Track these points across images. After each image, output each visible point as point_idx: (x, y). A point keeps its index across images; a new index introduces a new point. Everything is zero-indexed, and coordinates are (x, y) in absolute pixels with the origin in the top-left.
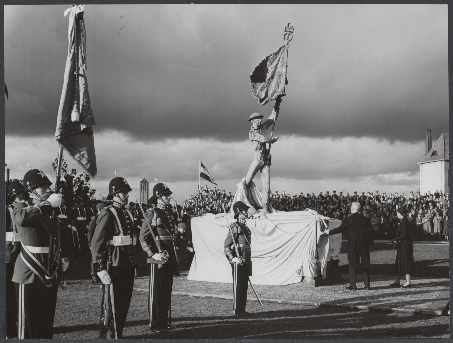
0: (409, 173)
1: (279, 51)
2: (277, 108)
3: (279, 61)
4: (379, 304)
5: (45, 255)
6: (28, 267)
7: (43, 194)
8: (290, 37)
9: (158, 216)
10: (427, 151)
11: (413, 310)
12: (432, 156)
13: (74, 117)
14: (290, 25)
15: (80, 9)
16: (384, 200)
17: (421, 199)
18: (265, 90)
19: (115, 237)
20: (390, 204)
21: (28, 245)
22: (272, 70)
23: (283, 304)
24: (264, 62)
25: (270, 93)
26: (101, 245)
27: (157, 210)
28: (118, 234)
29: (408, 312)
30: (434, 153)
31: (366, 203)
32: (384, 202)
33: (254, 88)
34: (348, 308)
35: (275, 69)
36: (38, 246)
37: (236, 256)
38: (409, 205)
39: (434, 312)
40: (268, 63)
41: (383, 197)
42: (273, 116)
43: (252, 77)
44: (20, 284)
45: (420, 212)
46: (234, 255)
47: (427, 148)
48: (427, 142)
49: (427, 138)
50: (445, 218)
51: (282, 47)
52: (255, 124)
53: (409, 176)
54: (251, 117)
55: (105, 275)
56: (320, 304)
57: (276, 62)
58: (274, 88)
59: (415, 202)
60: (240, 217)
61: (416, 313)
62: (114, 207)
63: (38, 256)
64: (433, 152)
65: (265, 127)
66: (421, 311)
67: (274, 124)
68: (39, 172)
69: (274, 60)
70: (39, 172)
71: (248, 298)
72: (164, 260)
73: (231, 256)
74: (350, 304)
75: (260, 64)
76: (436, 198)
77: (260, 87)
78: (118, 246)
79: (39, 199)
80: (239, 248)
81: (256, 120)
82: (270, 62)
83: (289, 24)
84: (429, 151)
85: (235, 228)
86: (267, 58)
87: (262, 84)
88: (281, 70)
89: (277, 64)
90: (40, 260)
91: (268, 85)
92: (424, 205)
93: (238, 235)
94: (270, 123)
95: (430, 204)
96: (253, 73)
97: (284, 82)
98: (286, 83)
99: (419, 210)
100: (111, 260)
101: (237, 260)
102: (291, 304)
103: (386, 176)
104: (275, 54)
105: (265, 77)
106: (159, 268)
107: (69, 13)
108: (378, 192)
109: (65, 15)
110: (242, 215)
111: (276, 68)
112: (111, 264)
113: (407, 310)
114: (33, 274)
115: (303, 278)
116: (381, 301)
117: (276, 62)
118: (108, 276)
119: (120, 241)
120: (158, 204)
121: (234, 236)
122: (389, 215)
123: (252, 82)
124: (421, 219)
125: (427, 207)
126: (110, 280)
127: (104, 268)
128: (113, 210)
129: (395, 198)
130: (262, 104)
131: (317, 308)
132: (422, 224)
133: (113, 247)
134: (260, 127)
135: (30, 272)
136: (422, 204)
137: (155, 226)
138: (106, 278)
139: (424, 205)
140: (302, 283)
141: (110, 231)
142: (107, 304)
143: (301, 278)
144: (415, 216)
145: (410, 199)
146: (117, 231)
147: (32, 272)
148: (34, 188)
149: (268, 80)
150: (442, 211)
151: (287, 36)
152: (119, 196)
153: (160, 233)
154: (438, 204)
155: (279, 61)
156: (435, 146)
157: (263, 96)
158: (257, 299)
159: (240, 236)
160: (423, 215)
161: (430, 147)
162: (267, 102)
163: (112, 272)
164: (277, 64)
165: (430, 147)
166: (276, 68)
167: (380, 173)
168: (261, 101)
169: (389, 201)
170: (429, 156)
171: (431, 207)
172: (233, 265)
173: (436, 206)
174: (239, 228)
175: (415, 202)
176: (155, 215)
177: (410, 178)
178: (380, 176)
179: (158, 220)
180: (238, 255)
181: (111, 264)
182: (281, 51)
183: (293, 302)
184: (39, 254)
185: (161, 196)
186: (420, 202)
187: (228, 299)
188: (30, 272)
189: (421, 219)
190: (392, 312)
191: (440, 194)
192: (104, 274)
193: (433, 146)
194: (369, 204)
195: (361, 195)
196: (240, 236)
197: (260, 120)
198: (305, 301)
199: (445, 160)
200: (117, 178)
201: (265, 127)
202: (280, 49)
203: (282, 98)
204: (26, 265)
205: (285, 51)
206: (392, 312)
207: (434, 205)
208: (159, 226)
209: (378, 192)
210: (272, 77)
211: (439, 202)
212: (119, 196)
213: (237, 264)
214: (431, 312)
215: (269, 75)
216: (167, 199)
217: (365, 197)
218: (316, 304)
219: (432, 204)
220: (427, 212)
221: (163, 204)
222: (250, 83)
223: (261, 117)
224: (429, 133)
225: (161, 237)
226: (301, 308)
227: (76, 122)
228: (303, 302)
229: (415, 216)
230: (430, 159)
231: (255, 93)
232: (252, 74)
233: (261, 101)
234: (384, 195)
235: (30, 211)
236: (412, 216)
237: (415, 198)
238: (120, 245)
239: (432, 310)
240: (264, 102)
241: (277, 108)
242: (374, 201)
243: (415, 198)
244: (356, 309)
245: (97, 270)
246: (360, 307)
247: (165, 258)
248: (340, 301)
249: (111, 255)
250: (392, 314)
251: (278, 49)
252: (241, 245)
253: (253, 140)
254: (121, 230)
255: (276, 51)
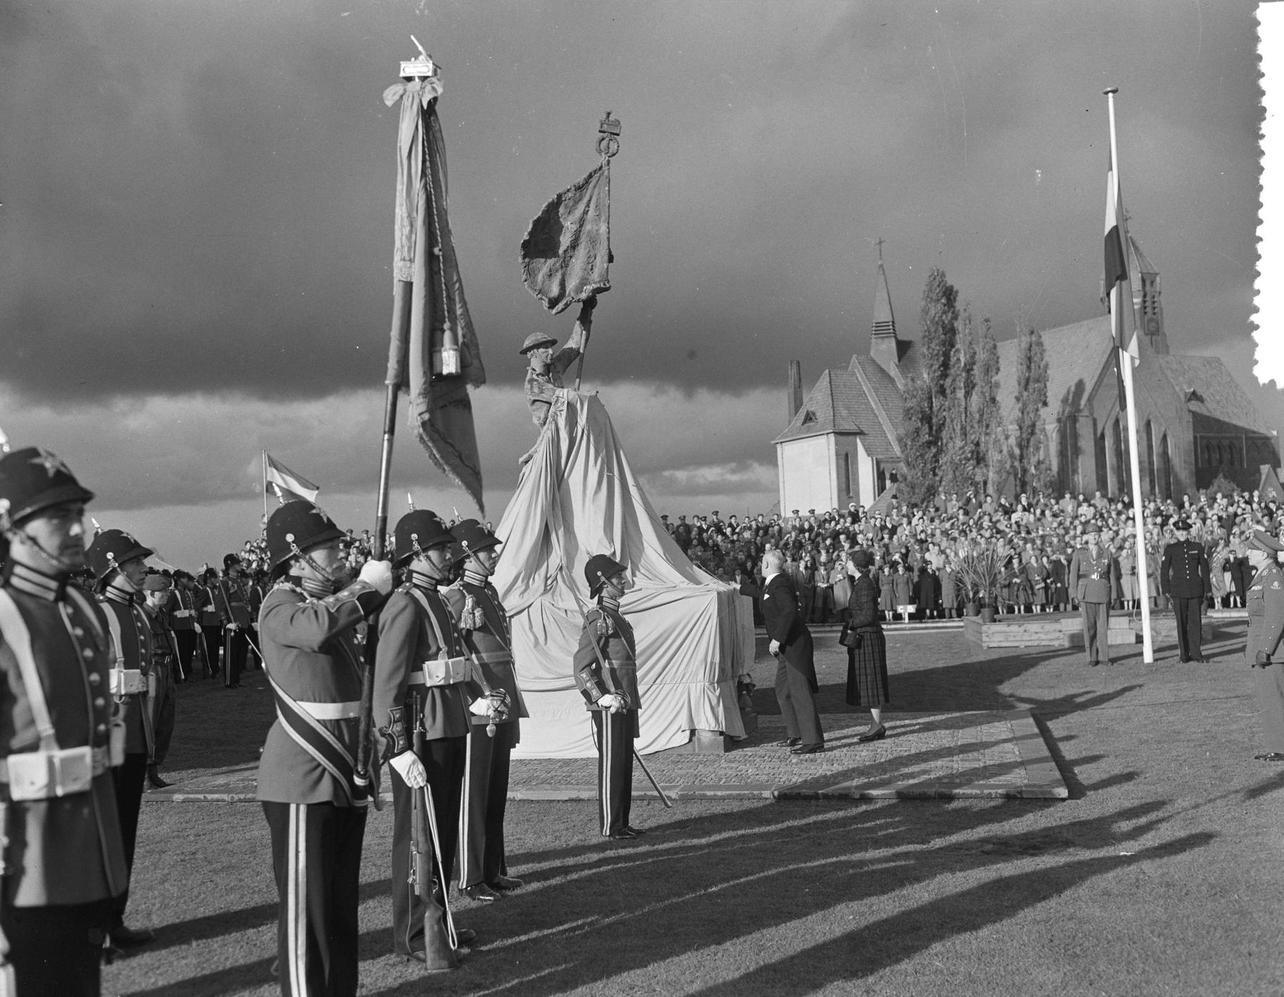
0: (733, 465)
1: (587, 181)
2: (585, 319)
3: (588, 205)
4: (911, 782)
5: (352, 723)
6: (313, 759)
7: (330, 564)
8: (613, 146)
9: (477, 604)
10: (793, 412)
11: (1000, 791)
12: (805, 422)
13: (449, 362)
14: (611, 118)
15: (434, 89)
16: (733, 532)
17: (819, 527)
18: (559, 275)
19: (428, 665)
20: (749, 542)
21: (308, 700)
22: (575, 227)
23: (685, 799)
24: (553, 207)
25: (571, 285)
26: (401, 686)
27: (468, 587)
28: (434, 657)
29: (989, 797)
30: (809, 418)
31: (695, 542)
32: (735, 537)
33: (531, 273)
34: (845, 799)
35: (581, 226)
36: (334, 701)
37: (608, 692)
38: (794, 543)
39: (1050, 792)
40: (561, 210)
41: (730, 525)
42: (576, 340)
43: (525, 245)
44: (293, 808)
45: (823, 558)
46: (604, 691)
47: (792, 405)
48: (792, 390)
49: (791, 381)
50: (881, 568)
51: (595, 172)
52: (537, 361)
53: (733, 472)
54: (527, 343)
55: (414, 763)
56: (776, 793)
57: (581, 207)
58: (579, 275)
59: (807, 535)
60: (604, 593)
61: (1008, 797)
62: (416, 586)
63: (334, 726)
64: (808, 414)
65: (560, 367)
66: (1020, 792)
67: (581, 360)
68: (313, 508)
69: (576, 202)
70: (313, 508)
71: (510, 795)
72: (501, 713)
73: (595, 693)
74: (849, 788)
75: (545, 212)
76: (853, 523)
77: (545, 270)
78: (437, 687)
79: (320, 577)
80: (613, 671)
81: (541, 350)
82: (566, 207)
83: (609, 114)
84: (796, 412)
85: (600, 622)
86: (559, 196)
87: (551, 262)
88: (595, 228)
89: (585, 212)
90: (340, 738)
91: (565, 265)
92: (828, 542)
93: (608, 638)
94: (573, 354)
95: (842, 537)
96: (531, 234)
97: (606, 258)
98: (611, 259)
99: (819, 552)
100: (422, 724)
101: (610, 702)
102: (703, 798)
103: (681, 475)
104: (580, 188)
105: (557, 244)
106: (490, 735)
107: (402, 97)
108: (716, 513)
109: (389, 103)
110: (610, 588)
111: (582, 222)
112: (423, 735)
113: (986, 791)
114: (326, 774)
115: (693, 732)
116: (912, 776)
117: (581, 207)
118: (421, 767)
119: (442, 674)
120: (467, 573)
121: (598, 643)
122: (753, 568)
123: (524, 257)
124: (828, 574)
125: (836, 545)
126: (425, 775)
127: (409, 747)
128: (418, 594)
129: (758, 529)
130: (554, 311)
131: (771, 805)
132: (831, 587)
133: (423, 689)
134: (548, 368)
135: (320, 769)
136: (824, 540)
137: (468, 630)
138: (416, 773)
139: (828, 542)
140: (689, 746)
141: (417, 650)
142: (421, 839)
143: (688, 733)
144: (813, 568)
145: (794, 527)
146: (434, 649)
147: (324, 769)
148: (306, 550)
149: (565, 251)
150: (872, 554)
151: (604, 143)
152: (428, 558)
153: (480, 647)
154: (860, 538)
155: (588, 205)
156: (811, 399)
157: (555, 291)
158: (656, 793)
159: (611, 640)
160: (831, 563)
161: (798, 403)
162: (567, 305)
163: (426, 755)
164: (585, 212)
165: (798, 403)
166: (582, 222)
167: (665, 468)
168: (553, 303)
169: (747, 535)
170: (799, 423)
171: (847, 546)
172: (597, 716)
173: (857, 543)
174: (609, 621)
175: (807, 535)
176: (469, 601)
177: (735, 478)
178: (666, 473)
179: (478, 613)
180: (613, 689)
181: (423, 735)
182: (594, 180)
183: (709, 793)
184: (338, 721)
185: (475, 553)
186: (818, 534)
187: (538, 801)
188: (320, 769)
189: (828, 574)
190: (951, 798)
191: (861, 515)
192: (410, 762)
193: (805, 400)
194: (703, 543)
195: (679, 522)
196: (611, 640)
197: (550, 351)
198: (736, 788)
199: (838, 434)
200: (416, 512)
201: (560, 367)
202: (590, 176)
203: (598, 297)
204: (306, 752)
205: (603, 180)
206: (951, 798)
207: (853, 539)
208: (479, 629)
209: (716, 513)
210: (574, 246)
211: (861, 532)
212: (428, 558)
213: (613, 710)
214: (1042, 793)
215: (565, 240)
216: (490, 558)
217: (688, 529)
218: (767, 794)
219: (848, 538)
220: (838, 556)
221: (481, 572)
222: (520, 260)
223: (553, 343)
224: (795, 367)
225: (484, 655)
226: (735, 807)
227: (450, 376)
228: (734, 792)
229: (813, 568)
230: (800, 431)
231: (533, 283)
232: (526, 237)
233: (553, 303)
234: (733, 520)
235: (338, 610)
236: (806, 568)
237: (806, 526)
238: (442, 683)
239: (1041, 786)
240: (560, 306)
241: (585, 319)
242: (711, 537)
243: (806, 526)
244: (866, 799)
245: (391, 753)
246: (874, 792)
247: (502, 708)
248: (817, 782)
249: (422, 711)
250: (955, 805)
251: (585, 176)
252: (616, 663)
253: (535, 401)
254: (442, 645)
255: (580, 180)
